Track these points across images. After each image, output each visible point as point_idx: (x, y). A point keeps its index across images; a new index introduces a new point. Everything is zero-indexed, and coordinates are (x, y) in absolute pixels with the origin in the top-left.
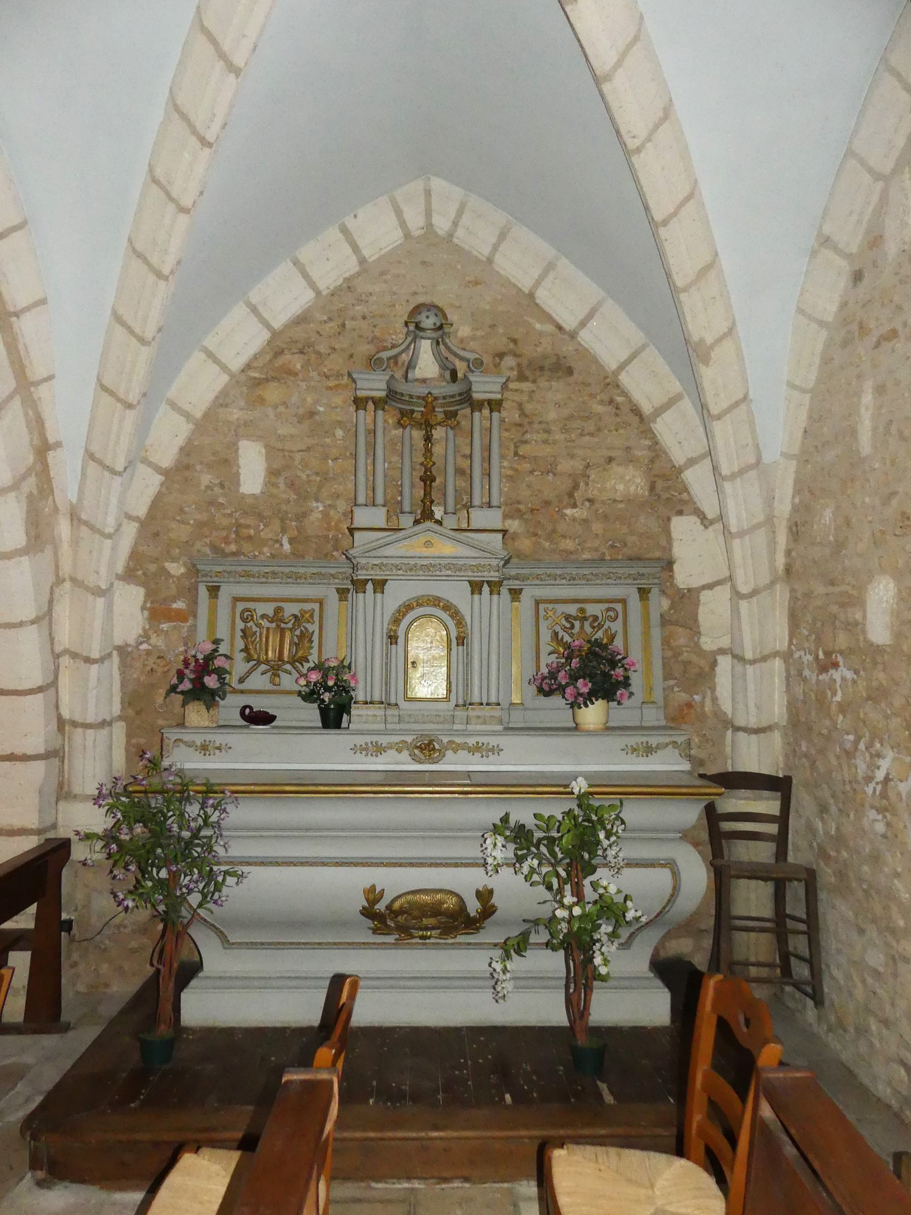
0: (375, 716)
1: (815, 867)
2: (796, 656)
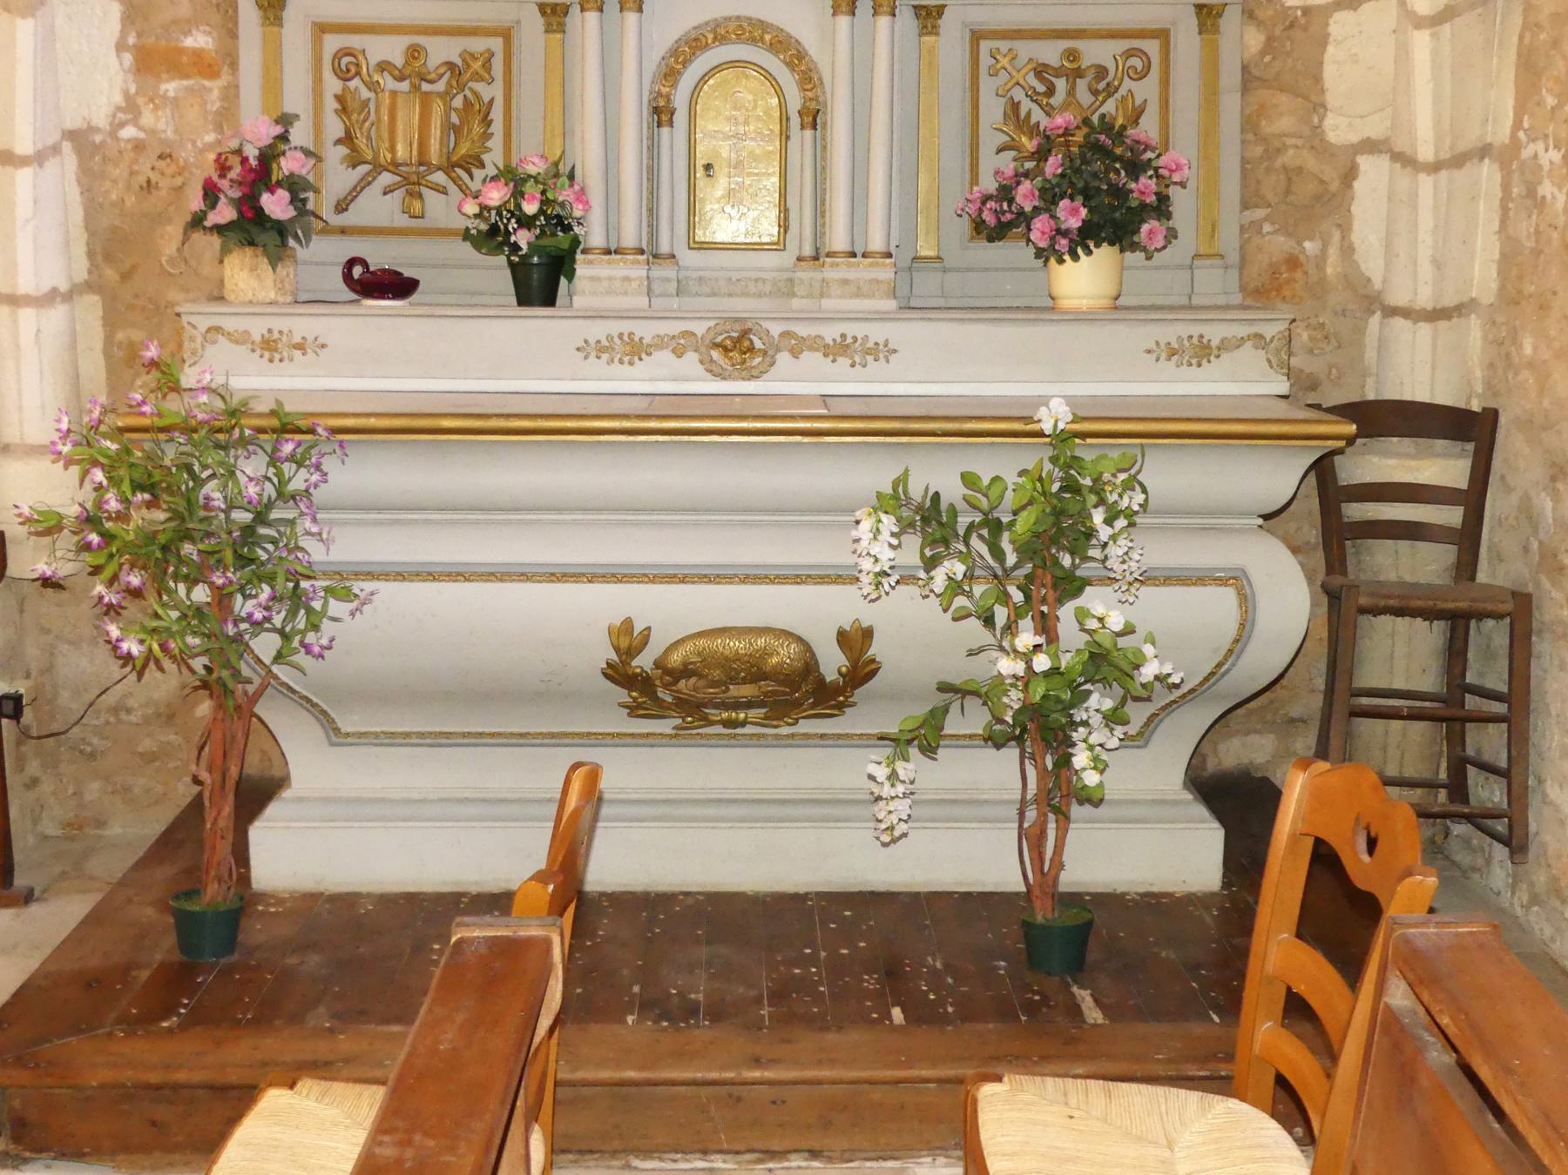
0: (627, 279)
1: (1530, 589)
2: (1526, 153)
